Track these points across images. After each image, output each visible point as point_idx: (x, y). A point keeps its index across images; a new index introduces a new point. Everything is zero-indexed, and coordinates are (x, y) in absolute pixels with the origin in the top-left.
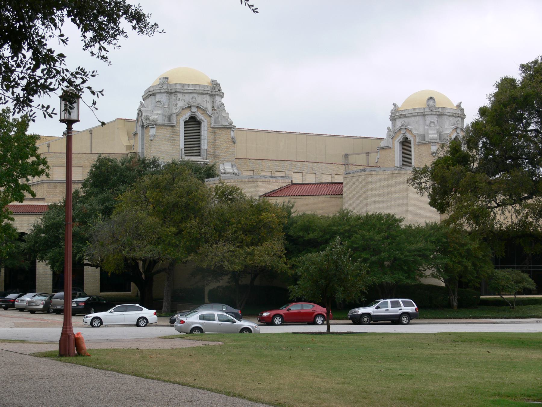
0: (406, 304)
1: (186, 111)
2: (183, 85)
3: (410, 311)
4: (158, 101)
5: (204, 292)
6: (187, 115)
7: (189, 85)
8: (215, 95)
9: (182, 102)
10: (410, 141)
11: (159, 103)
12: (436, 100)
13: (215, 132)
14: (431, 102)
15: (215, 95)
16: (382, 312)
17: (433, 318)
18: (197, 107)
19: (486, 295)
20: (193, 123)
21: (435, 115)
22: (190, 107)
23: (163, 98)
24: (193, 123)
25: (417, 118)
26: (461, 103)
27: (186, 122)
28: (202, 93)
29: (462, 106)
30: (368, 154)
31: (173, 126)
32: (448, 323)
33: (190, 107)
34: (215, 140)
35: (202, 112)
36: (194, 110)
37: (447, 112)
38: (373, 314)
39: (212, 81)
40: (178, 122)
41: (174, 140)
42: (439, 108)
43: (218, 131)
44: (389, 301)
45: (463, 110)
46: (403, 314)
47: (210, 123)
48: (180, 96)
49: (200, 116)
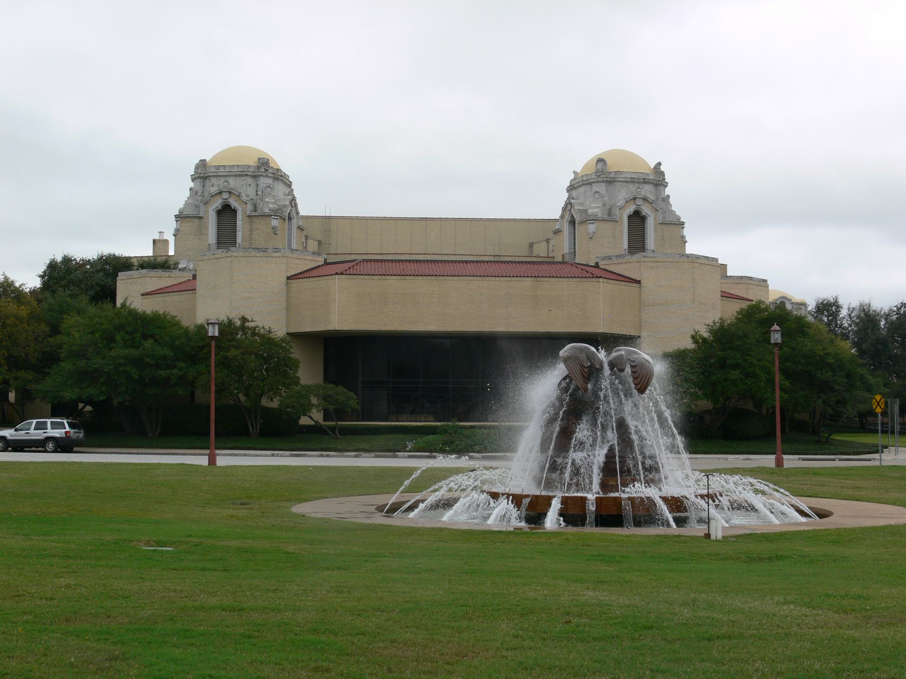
0: (55, 426)
1: (216, 198)
2: (218, 167)
3: (58, 435)
4: (597, 192)
5: (460, 452)
6: (631, 209)
7: (225, 166)
8: (259, 176)
9: (622, 194)
10: (235, 212)
11: (597, 195)
12: (608, 162)
13: (251, 222)
14: (600, 165)
15: (259, 176)
16: (21, 435)
17: (125, 447)
18: (230, 193)
19: (363, 421)
20: (637, 219)
21: (603, 182)
22: (635, 199)
23: (601, 188)
24: (637, 219)
25: (583, 188)
26: (659, 164)
27: (630, 217)
28: (240, 175)
29: (662, 168)
30: (548, 241)
31: (200, 218)
32: (138, 454)
33: (635, 199)
34: (251, 231)
35: (236, 198)
36: (639, 202)
37: (621, 177)
38: (9, 438)
39: (259, 159)
40: (207, 212)
41: (201, 234)
42: (610, 173)
43: (255, 220)
44: (49, 421)
45: (662, 173)
46: (48, 439)
47: (244, 211)
48: (214, 180)
49: (234, 203)
